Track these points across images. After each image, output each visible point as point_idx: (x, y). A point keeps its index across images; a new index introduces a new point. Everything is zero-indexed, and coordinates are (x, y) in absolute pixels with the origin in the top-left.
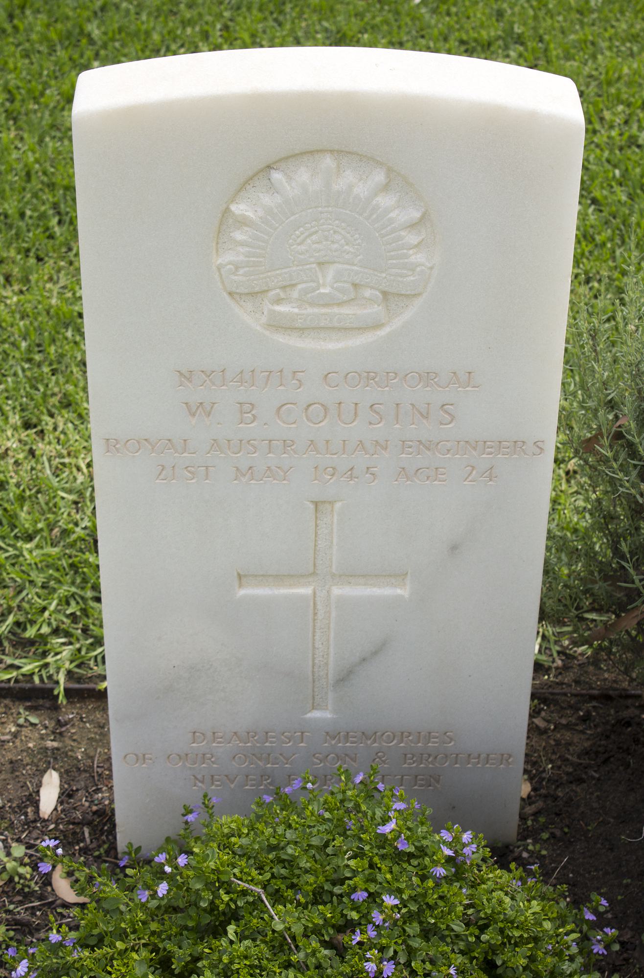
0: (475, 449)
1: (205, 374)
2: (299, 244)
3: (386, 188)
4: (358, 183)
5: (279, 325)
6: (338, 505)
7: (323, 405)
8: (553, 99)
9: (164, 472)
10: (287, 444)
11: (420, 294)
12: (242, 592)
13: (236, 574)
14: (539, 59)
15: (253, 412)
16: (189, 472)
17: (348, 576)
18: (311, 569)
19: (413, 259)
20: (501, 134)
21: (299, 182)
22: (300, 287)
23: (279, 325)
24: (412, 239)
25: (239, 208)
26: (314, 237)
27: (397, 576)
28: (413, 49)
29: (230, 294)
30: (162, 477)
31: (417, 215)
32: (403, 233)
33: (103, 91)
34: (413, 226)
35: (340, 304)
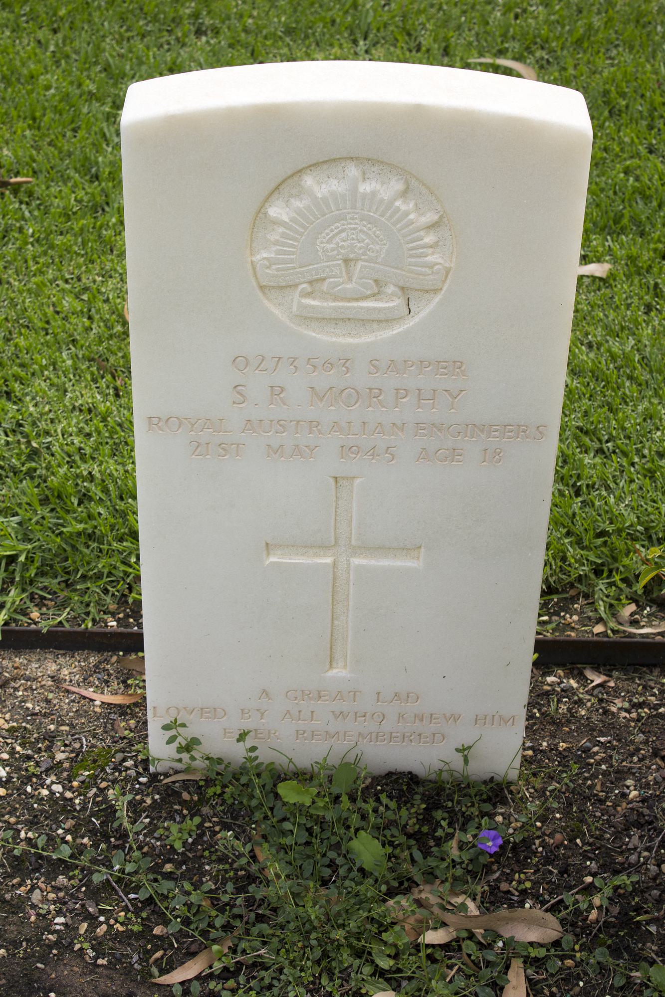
0: (482, 431)
1: (451, 395)
2: (328, 242)
3: (404, 194)
4: (381, 188)
5: (307, 318)
6: (357, 481)
7: (357, 392)
8: (564, 110)
9: (199, 449)
10: (313, 425)
11: (436, 291)
12: (273, 559)
13: (264, 544)
14: (551, 71)
15: (282, 396)
16: (222, 448)
17: (366, 549)
18: (333, 543)
19: (430, 259)
20: (515, 140)
21: (321, 187)
22: (328, 281)
23: (307, 318)
24: (429, 239)
25: (277, 211)
26: (344, 235)
27: (408, 549)
28: (427, 64)
29: (262, 288)
30: (196, 453)
31: (436, 217)
32: (422, 233)
33: (148, 101)
34: (433, 226)
35: (365, 298)
